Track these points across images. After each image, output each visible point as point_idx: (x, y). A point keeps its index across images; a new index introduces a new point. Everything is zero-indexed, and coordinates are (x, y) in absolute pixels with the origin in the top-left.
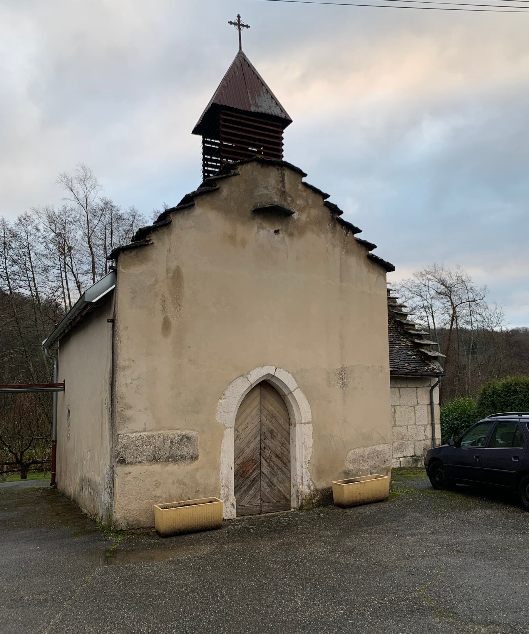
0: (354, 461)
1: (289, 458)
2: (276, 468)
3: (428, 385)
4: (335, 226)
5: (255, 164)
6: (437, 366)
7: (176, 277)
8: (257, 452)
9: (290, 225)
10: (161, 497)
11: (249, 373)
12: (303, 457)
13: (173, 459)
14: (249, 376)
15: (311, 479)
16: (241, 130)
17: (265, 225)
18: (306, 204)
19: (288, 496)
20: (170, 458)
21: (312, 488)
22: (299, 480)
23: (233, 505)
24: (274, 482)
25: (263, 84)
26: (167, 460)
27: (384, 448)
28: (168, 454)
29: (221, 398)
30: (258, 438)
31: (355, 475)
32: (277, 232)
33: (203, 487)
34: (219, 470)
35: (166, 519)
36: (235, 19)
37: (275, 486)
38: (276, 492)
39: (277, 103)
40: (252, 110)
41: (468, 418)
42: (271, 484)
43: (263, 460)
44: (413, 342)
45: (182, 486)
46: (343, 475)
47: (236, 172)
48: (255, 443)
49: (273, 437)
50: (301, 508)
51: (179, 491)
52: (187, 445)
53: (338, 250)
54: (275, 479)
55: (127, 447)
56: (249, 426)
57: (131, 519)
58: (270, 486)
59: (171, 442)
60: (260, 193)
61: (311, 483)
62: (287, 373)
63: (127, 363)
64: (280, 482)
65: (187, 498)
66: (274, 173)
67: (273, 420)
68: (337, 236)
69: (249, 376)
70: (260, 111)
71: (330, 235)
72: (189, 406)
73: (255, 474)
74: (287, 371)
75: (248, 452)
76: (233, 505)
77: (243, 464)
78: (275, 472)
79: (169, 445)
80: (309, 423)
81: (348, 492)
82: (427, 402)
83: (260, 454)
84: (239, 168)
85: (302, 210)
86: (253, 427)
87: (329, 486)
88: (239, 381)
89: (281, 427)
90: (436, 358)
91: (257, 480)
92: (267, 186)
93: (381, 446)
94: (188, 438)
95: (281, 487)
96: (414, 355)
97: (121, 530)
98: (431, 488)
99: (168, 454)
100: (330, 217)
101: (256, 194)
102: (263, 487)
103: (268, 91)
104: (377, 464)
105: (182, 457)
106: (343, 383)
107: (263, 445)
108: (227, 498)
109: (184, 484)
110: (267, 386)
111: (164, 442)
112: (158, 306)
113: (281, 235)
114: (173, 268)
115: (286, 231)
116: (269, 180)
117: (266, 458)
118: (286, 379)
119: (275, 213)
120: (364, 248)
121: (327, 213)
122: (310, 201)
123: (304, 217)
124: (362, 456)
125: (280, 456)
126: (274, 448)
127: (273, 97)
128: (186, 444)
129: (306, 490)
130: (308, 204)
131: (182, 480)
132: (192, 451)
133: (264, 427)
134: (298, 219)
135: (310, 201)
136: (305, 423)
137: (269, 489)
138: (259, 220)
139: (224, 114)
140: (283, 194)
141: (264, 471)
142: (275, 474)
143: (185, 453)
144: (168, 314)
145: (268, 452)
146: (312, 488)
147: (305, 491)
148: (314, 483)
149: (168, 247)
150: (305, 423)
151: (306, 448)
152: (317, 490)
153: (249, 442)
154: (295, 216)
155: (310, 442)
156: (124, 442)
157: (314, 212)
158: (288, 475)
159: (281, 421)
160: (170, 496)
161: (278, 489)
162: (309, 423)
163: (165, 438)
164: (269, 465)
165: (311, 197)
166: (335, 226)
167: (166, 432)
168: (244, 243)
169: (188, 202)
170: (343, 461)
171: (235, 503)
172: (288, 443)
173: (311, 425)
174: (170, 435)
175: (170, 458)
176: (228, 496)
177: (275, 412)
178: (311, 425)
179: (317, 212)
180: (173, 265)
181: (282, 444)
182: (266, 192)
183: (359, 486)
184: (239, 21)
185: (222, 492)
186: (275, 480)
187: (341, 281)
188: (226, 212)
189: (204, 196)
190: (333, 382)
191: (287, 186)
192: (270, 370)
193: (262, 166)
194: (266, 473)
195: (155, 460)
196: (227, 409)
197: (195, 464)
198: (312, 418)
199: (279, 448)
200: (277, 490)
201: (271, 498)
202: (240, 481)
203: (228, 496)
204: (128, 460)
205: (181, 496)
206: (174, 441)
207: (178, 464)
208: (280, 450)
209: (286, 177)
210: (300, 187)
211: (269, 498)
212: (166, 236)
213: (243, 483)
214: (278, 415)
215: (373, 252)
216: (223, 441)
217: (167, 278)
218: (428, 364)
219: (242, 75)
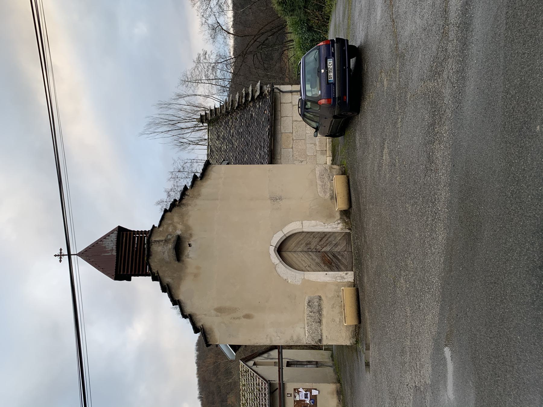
0: (325, 192)
3: (279, 94)
4: (183, 204)
5: (150, 260)
6: (267, 89)
7: (220, 310)
9: (185, 236)
11: (273, 264)
13: (320, 311)
16: (126, 255)
17: (186, 254)
19: (343, 234)
21: (339, 222)
23: (346, 274)
25: (97, 243)
26: (321, 315)
30: (310, 253)
32: (190, 245)
34: (327, 282)
38: (341, 242)
39: (108, 235)
40: (115, 254)
42: (336, 245)
47: (156, 273)
55: (313, 338)
56: (303, 259)
57: (351, 336)
61: (336, 222)
68: (189, 202)
71: (189, 208)
75: (318, 260)
76: (346, 274)
77: (324, 263)
80: (302, 223)
81: (341, 204)
84: (154, 271)
85: (175, 228)
90: (261, 88)
92: (161, 252)
94: (309, 302)
99: (317, 314)
100: (178, 208)
101: (168, 260)
103: (101, 240)
105: (319, 305)
107: (314, 250)
108: (343, 278)
109: (333, 304)
111: (311, 316)
113: (191, 242)
114: (215, 312)
115: (189, 239)
116: (159, 251)
119: (179, 247)
121: (176, 209)
122: (169, 222)
123: (180, 226)
124: (322, 187)
126: (316, 243)
127: (105, 237)
129: (340, 226)
130: (171, 224)
134: (181, 230)
135: (169, 222)
137: (339, 246)
138: (184, 258)
139: (120, 271)
140: (166, 241)
143: (317, 304)
145: (318, 247)
148: (337, 220)
151: (316, 225)
152: (341, 218)
153: (312, 259)
155: (313, 222)
156: (310, 340)
157: (176, 219)
159: (301, 238)
162: (302, 223)
164: (326, 246)
166: (183, 204)
167: (306, 315)
168: (198, 268)
169: (175, 302)
171: (345, 272)
173: (304, 222)
176: (341, 277)
178: (304, 222)
179: (175, 217)
180: (213, 312)
182: (166, 253)
184: (58, 255)
185: (339, 281)
187: (218, 199)
188: (180, 279)
192: (272, 249)
193: (151, 255)
195: (320, 322)
196: (293, 277)
197: (323, 298)
202: (334, 265)
203: (341, 277)
204: (320, 338)
209: (156, 239)
210: (161, 229)
212: (198, 317)
215: (198, 175)
219: (93, 254)
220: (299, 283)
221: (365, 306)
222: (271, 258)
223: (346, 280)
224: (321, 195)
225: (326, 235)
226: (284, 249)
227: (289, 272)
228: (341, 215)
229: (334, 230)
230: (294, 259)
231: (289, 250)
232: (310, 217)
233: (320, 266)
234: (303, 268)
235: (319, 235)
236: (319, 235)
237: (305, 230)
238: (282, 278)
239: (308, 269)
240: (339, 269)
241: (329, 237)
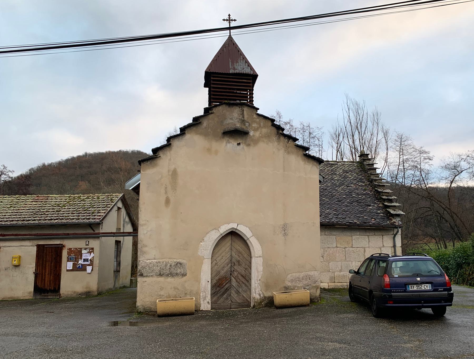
0: (292, 281)
5: (224, 106)
6: (397, 221)
7: (174, 174)
8: (229, 273)
11: (219, 227)
13: (171, 275)
14: (219, 229)
16: (230, 83)
17: (230, 140)
18: (258, 126)
19: (249, 300)
21: (262, 295)
23: (208, 302)
24: (240, 291)
25: (242, 54)
27: (314, 274)
30: (230, 265)
32: (239, 144)
35: (162, 307)
36: (227, 17)
37: (240, 293)
39: (249, 65)
40: (231, 72)
41: (467, 257)
42: (238, 292)
44: (383, 204)
46: (284, 289)
47: (212, 111)
48: (227, 268)
49: (239, 265)
50: (254, 306)
53: (282, 152)
54: (241, 289)
55: (144, 268)
56: (224, 258)
57: (146, 306)
58: (237, 293)
60: (227, 123)
61: (261, 293)
63: (144, 222)
66: (237, 110)
67: (240, 255)
68: (281, 143)
69: (219, 229)
70: (235, 72)
73: (227, 286)
75: (222, 273)
76: (208, 302)
80: (260, 257)
82: (391, 245)
83: (231, 274)
85: (256, 130)
88: (213, 232)
90: (398, 215)
93: (312, 272)
94: (180, 264)
96: (382, 213)
97: (140, 312)
98: (349, 301)
99: (168, 272)
100: (276, 133)
103: (244, 58)
104: (310, 283)
105: (177, 274)
106: (285, 233)
108: (205, 299)
110: (233, 234)
112: (163, 191)
113: (242, 145)
114: (172, 169)
115: (245, 143)
118: (244, 230)
120: (302, 150)
121: (274, 130)
122: (262, 124)
123: (257, 134)
124: (298, 278)
126: (240, 271)
127: (247, 62)
129: (257, 297)
130: (260, 126)
135: (262, 124)
136: (257, 257)
137: (236, 295)
138: (226, 139)
139: (214, 77)
140: (243, 121)
143: (178, 272)
145: (236, 274)
148: (263, 293)
149: (169, 157)
150: (257, 257)
151: (258, 272)
152: (265, 297)
154: (251, 133)
155: (261, 268)
156: (143, 265)
157: (264, 130)
159: (245, 256)
162: (260, 257)
164: (237, 281)
165: (263, 122)
167: (167, 260)
168: (216, 152)
171: (210, 302)
173: (261, 258)
177: (241, 250)
178: (261, 258)
179: (267, 130)
180: (172, 168)
182: (231, 121)
183: (287, 295)
184: (229, 18)
185: (201, 295)
186: (240, 290)
187: (284, 171)
188: (206, 135)
189: (192, 128)
191: (246, 117)
192: (234, 226)
193: (229, 107)
194: (235, 286)
195: (161, 275)
197: (185, 278)
204: (145, 274)
209: (245, 112)
210: (255, 116)
218: (391, 219)
219: (230, 50)
220: (199, 253)
222: (225, 225)
223: (202, 302)
224: (289, 276)
226: (233, 237)
228: (269, 297)
229: (253, 290)
230: (223, 249)
232: (266, 264)
233: (216, 275)
235: (248, 274)
236: (248, 274)
237: (253, 260)
238: (205, 236)
239: (214, 263)
240: (213, 295)
241: (246, 285)
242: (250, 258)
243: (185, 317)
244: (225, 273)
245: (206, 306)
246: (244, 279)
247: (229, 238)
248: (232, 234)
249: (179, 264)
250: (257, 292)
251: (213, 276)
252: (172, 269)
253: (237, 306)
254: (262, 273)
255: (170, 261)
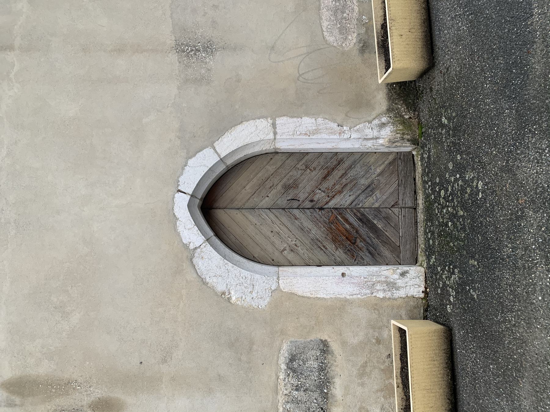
0: (344, 31)
1: (331, 155)
2: (344, 180)
8: (318, 214)
10: (383, 405)
11: (186, 246)
12: (332, 137)
13: (323, 385)
15: (370, 122)
19: (391, 158)
20: (322, 392)
21: (384, 120)
22: (369, 144)
23: (403, 274)
26: (325, 396)
28: (316, 395)
29: (229, 299)
30: (296, 212)
31: (368, 28)
33: (371, 331)
34: (346, 300)
37: (372, 182)
38: (382, 180)
42: (370, 189)
43: (330, 204)
45: (368, 370)
46: (366, 55)
51: (376, 373)
52: (303, 360)
56: (277, 229)
58: (373, 191)
59: (297, 390)
61: (376, 122)
62: (187, 168)
64: (367, 172)
65: (388, 361)
67: (269, 184)
69: (192, 247)
72: (240, 360)
73: (352, 219)
74: (183, 169)
75: (317, 232)
78: (351, 181)
79: (302, 393)
80: (274, 125)
83: (321, 209)
86: (278, 222)
87: (384, 87)
88: (199, 263)
89: (280, 171)
91: (363, 215)
94: (292, 359)
95: (375, 169)
99: (316, 395)
102: (373, 204)
105: (322, 369)
107: (308, 204)
108: (392, 285)
109: (365, 365)
110: (209, 205)
111: (296, 402)
117: (328, 199)
118: (196, 171)
125: (326, 172)
126: (313, 183)
128: (301, 363)
129: (387, 132)
131: (359, 370)
132: (313, 352)
133: (279, 202)
136: (275, 133)
137: (377, 193)
141: (348, 202)
142: (355, 182)
144: (85, 403)
145: (319, 195)
146: (384, 120)
147: (389, 133)
148: (378, 116)
150: (275, 133)
151: (317, 131)
155: (308, 122)
158: (357, 157)
159: (271, 169)
160: (382, 390)
161: (379, 175)
162: (274, 125)
163: (290, 400)
164: (340, 192)
167: (281, 399)
170: (343, 53)
172: (306, 158)
174: (285, 392)
175: (322, 392)
177: (255, 180)
181: (307, 167)
185: (381, 295)
186: (364, 182)
187: (11, 48)
190: (203, 71)
192: (181, 203)
194: (352, 198)
197: (334, 346)
198: (266, 117)
199: (314, 173)
200: (380, 178)
201: (392, 190)
205: (382, 370)
206: (296, 383)
207: (333, 378)
208: (317, 171)
211: (392, 193)
213: (365, 240)
214: (260, 175)
216: (300, 293)
217: (22, 405)
220: (263, 304)
221: (464, 382)
222: (180, 229)
223: (402, 293)
224: (331, 39)
225: (340, 162)
226: (222, 202)
227: (236, 270)
228: (390, 98)
229: (369, 146)
230: (251, 230)
231: (237, 204)
232: (296, 106)
233: (323, 248)
234: (277, 256)
235: (322, 160)
236: (322, 160)
237: (284, 145)
238: (213, 289)
239: (291, 256)
240: (376, 259)
241: (350, 168)
242: (277, 157)
243: (459, 359)
244: (316, 225)
245: (411, 282)
246: (336, 172)
247: (222, 215)
248: (212, 208)
249: (294, 363)
250: (375, 133)
251: (323, 258)
252: (308, 384)
253: (408, 191)
254: (320, 120)
255: (283, 390)
